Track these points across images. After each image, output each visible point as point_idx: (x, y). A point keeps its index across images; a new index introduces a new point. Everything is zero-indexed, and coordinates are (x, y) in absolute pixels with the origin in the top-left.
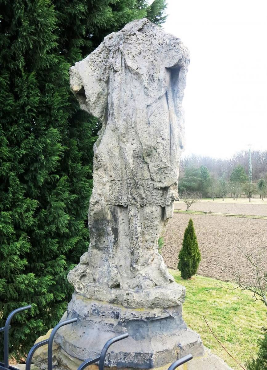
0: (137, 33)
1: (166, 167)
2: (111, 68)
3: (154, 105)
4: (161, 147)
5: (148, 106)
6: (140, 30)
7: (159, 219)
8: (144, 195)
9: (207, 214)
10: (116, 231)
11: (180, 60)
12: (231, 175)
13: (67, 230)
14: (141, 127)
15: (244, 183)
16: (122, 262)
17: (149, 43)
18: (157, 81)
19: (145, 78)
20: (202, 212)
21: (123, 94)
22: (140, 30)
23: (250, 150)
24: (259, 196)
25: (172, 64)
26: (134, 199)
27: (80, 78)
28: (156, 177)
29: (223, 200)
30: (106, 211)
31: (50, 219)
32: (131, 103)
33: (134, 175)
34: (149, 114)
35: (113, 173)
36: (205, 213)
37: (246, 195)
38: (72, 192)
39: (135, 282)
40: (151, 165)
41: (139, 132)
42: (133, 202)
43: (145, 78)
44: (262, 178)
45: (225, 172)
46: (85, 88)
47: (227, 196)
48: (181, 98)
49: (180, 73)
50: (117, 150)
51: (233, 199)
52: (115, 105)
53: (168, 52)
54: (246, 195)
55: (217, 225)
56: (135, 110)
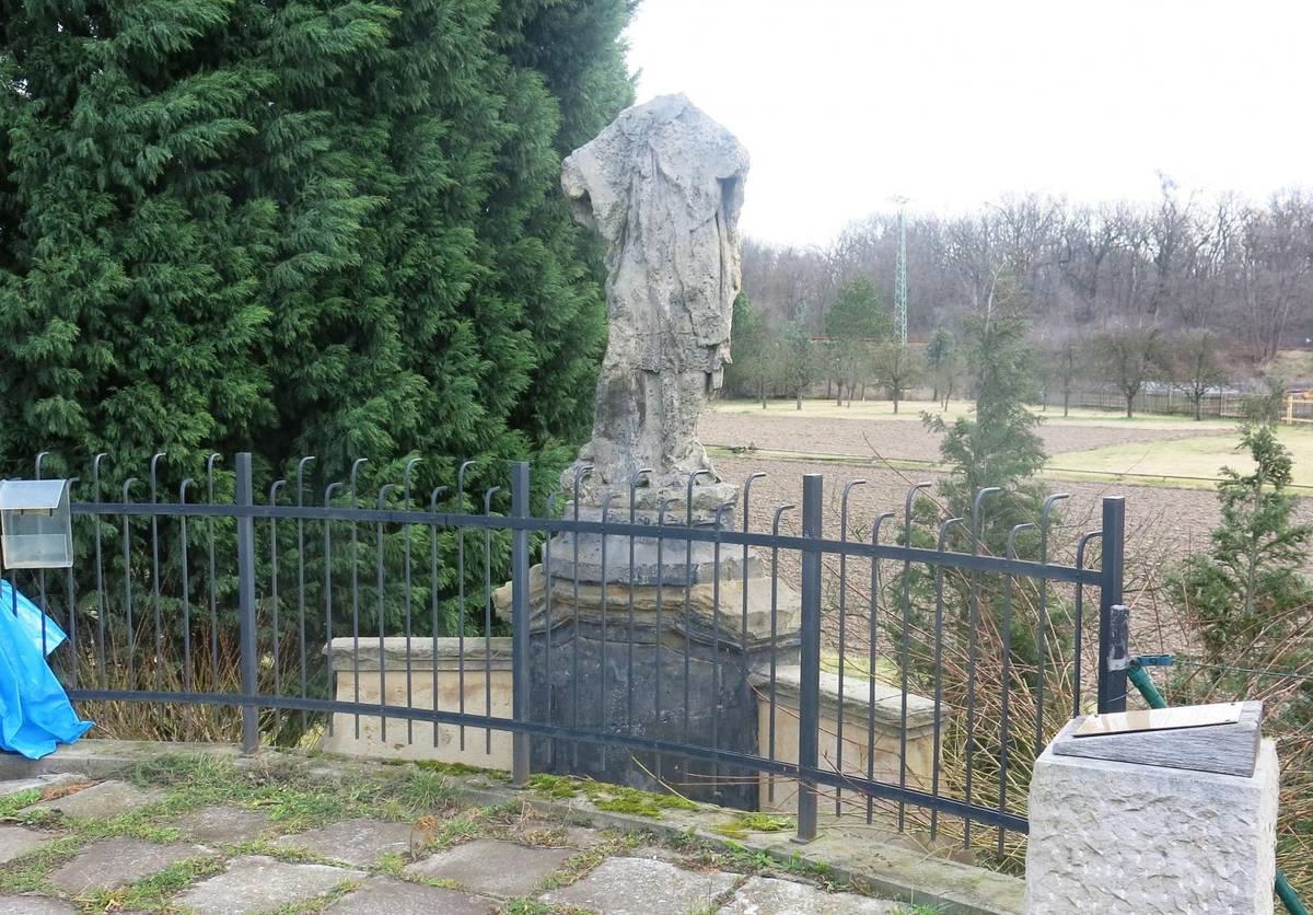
0: (675, 122)
1: (716, 317)
3: (700, 230)
4: (709, 289)
5: (691, 231)
6: (678, 117)
7: (702, 391)
8: (683, 356)
9: (741, 455)
10: (642, 407)
11: (737, 171)
12: (828, 311)
13: (473, 438)
14: (682, 260)
15: (878, 342)
16: (649, 453)
17: (691, 137)
18: (703, 196)
19: (689, 192)
20: (723, 448)
21: (655, 212)
22: (678, 117)
23: (900, 218)
24: (930, 393)
26: (670, 361)
27: (581, 178)
28: (701, 331)
29: (799, 408)
31: (442, 413)
32: (667, 225)
33: (670, 327)
35: (639, 325)
36: (734, 450)
37: (883, 389)
38: (484, 356)
39: (669, 478)
41: (679, 267)
42: (668, 365)
43: (689, 192)
44: (943, 324)
45: (809, 302)
47: (815, 391)
48: (736, 220)
50: (645, 291)
51: (835, 403)
52: (643, 226)
54: (883, 389)
55: (778, 490)
56: (674, 235)
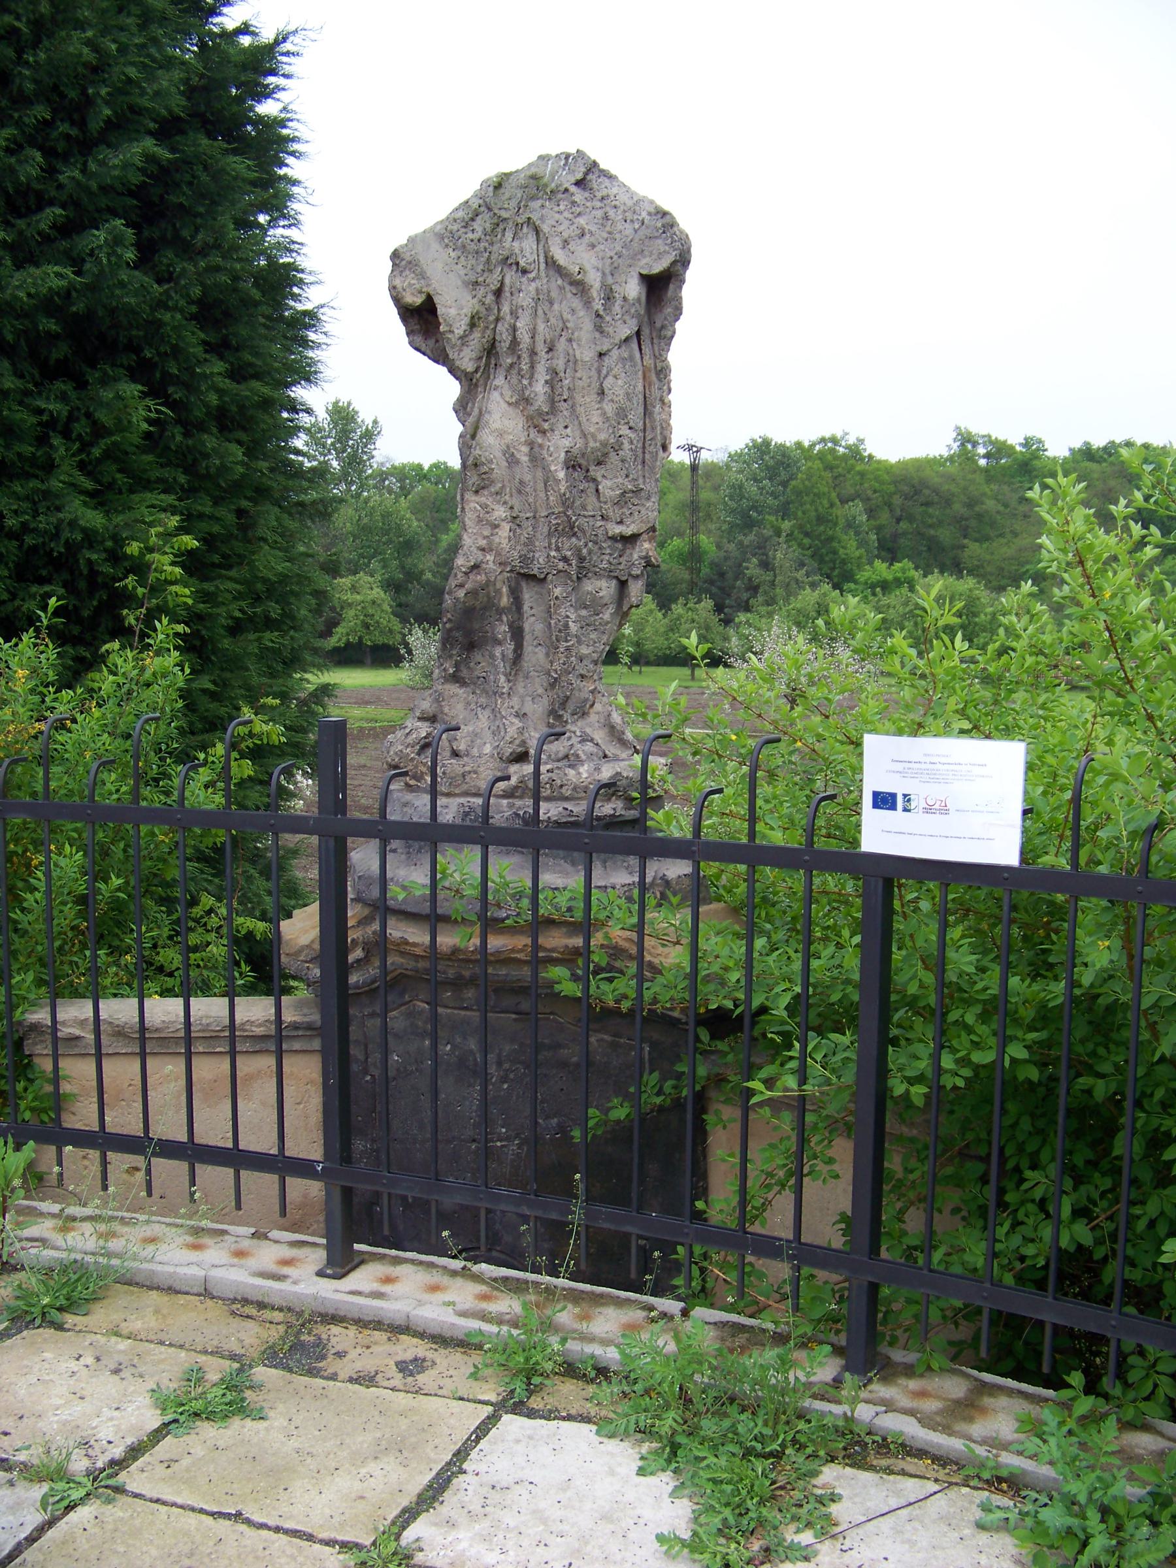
0: (573, 189)
2: (508, 261)
3: (615, 353)
5: (601, 355)
10: (517, 634)
22: (578, 183)
25: (657, 269)
30: (498, 586)
34: (604, 372)
35: (515, 501)
40: (605, 486)
42: (561, 565)
46: (436, 300)
49: (671, 286)
53: (647, 242)
